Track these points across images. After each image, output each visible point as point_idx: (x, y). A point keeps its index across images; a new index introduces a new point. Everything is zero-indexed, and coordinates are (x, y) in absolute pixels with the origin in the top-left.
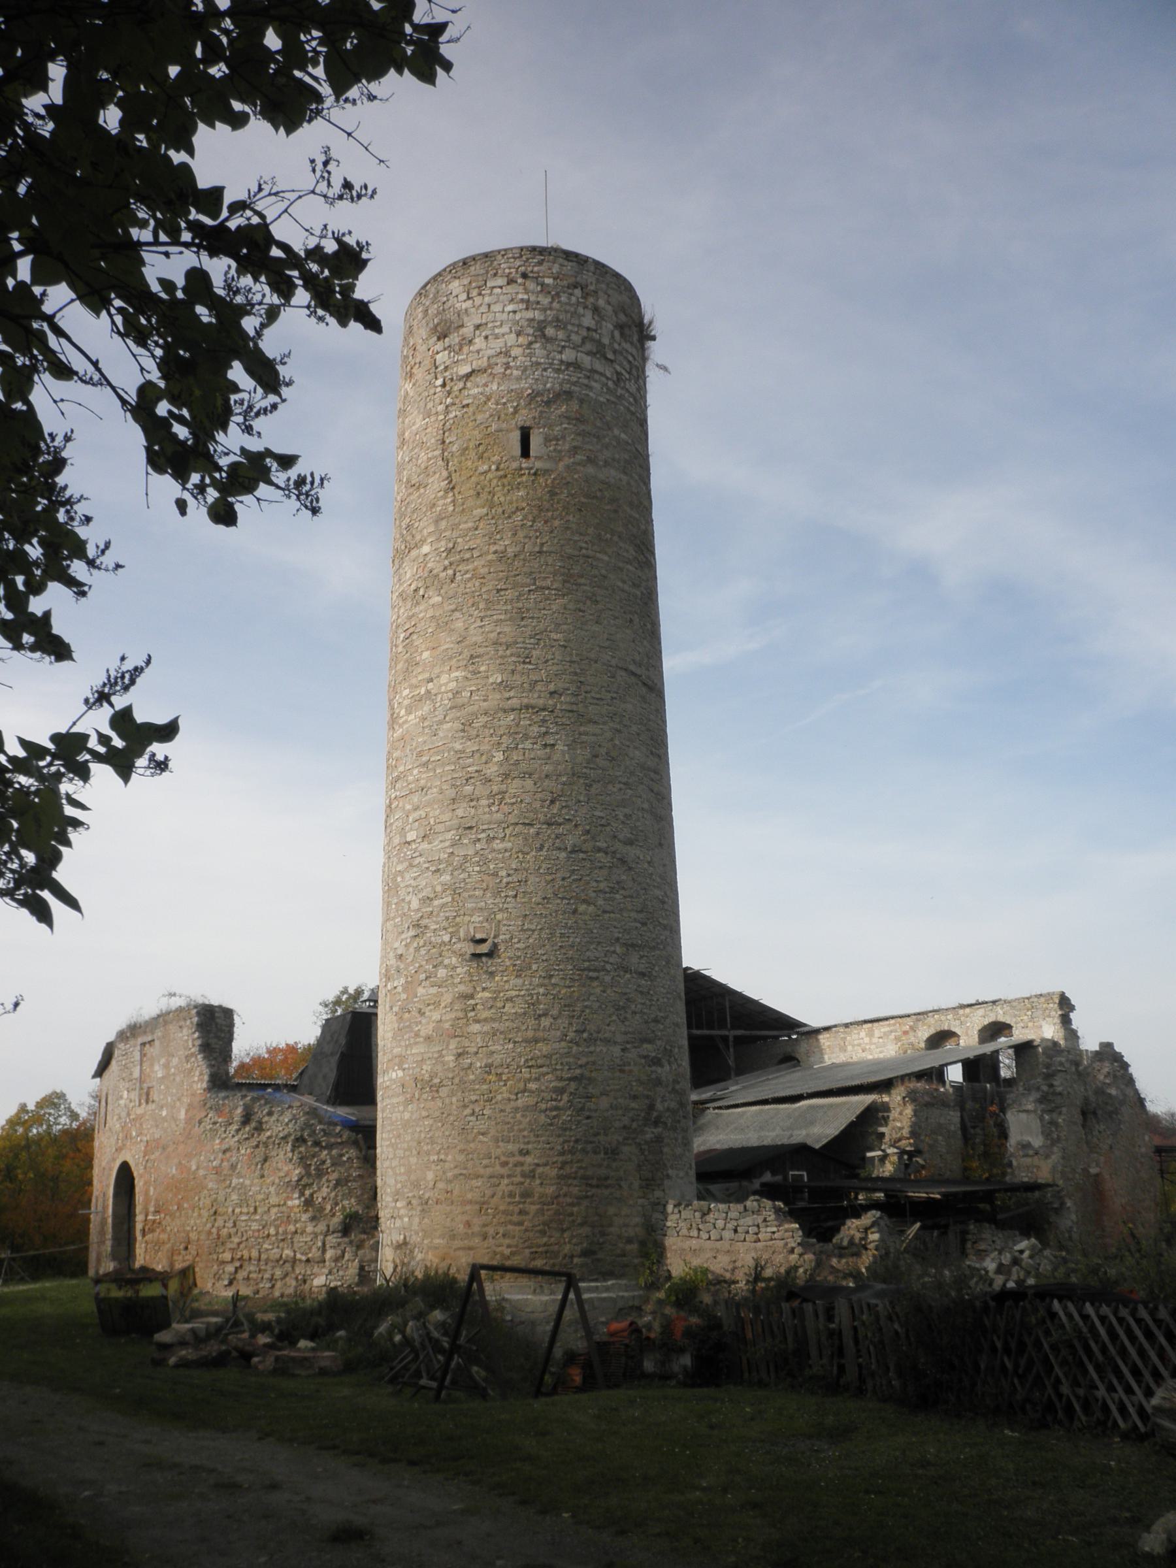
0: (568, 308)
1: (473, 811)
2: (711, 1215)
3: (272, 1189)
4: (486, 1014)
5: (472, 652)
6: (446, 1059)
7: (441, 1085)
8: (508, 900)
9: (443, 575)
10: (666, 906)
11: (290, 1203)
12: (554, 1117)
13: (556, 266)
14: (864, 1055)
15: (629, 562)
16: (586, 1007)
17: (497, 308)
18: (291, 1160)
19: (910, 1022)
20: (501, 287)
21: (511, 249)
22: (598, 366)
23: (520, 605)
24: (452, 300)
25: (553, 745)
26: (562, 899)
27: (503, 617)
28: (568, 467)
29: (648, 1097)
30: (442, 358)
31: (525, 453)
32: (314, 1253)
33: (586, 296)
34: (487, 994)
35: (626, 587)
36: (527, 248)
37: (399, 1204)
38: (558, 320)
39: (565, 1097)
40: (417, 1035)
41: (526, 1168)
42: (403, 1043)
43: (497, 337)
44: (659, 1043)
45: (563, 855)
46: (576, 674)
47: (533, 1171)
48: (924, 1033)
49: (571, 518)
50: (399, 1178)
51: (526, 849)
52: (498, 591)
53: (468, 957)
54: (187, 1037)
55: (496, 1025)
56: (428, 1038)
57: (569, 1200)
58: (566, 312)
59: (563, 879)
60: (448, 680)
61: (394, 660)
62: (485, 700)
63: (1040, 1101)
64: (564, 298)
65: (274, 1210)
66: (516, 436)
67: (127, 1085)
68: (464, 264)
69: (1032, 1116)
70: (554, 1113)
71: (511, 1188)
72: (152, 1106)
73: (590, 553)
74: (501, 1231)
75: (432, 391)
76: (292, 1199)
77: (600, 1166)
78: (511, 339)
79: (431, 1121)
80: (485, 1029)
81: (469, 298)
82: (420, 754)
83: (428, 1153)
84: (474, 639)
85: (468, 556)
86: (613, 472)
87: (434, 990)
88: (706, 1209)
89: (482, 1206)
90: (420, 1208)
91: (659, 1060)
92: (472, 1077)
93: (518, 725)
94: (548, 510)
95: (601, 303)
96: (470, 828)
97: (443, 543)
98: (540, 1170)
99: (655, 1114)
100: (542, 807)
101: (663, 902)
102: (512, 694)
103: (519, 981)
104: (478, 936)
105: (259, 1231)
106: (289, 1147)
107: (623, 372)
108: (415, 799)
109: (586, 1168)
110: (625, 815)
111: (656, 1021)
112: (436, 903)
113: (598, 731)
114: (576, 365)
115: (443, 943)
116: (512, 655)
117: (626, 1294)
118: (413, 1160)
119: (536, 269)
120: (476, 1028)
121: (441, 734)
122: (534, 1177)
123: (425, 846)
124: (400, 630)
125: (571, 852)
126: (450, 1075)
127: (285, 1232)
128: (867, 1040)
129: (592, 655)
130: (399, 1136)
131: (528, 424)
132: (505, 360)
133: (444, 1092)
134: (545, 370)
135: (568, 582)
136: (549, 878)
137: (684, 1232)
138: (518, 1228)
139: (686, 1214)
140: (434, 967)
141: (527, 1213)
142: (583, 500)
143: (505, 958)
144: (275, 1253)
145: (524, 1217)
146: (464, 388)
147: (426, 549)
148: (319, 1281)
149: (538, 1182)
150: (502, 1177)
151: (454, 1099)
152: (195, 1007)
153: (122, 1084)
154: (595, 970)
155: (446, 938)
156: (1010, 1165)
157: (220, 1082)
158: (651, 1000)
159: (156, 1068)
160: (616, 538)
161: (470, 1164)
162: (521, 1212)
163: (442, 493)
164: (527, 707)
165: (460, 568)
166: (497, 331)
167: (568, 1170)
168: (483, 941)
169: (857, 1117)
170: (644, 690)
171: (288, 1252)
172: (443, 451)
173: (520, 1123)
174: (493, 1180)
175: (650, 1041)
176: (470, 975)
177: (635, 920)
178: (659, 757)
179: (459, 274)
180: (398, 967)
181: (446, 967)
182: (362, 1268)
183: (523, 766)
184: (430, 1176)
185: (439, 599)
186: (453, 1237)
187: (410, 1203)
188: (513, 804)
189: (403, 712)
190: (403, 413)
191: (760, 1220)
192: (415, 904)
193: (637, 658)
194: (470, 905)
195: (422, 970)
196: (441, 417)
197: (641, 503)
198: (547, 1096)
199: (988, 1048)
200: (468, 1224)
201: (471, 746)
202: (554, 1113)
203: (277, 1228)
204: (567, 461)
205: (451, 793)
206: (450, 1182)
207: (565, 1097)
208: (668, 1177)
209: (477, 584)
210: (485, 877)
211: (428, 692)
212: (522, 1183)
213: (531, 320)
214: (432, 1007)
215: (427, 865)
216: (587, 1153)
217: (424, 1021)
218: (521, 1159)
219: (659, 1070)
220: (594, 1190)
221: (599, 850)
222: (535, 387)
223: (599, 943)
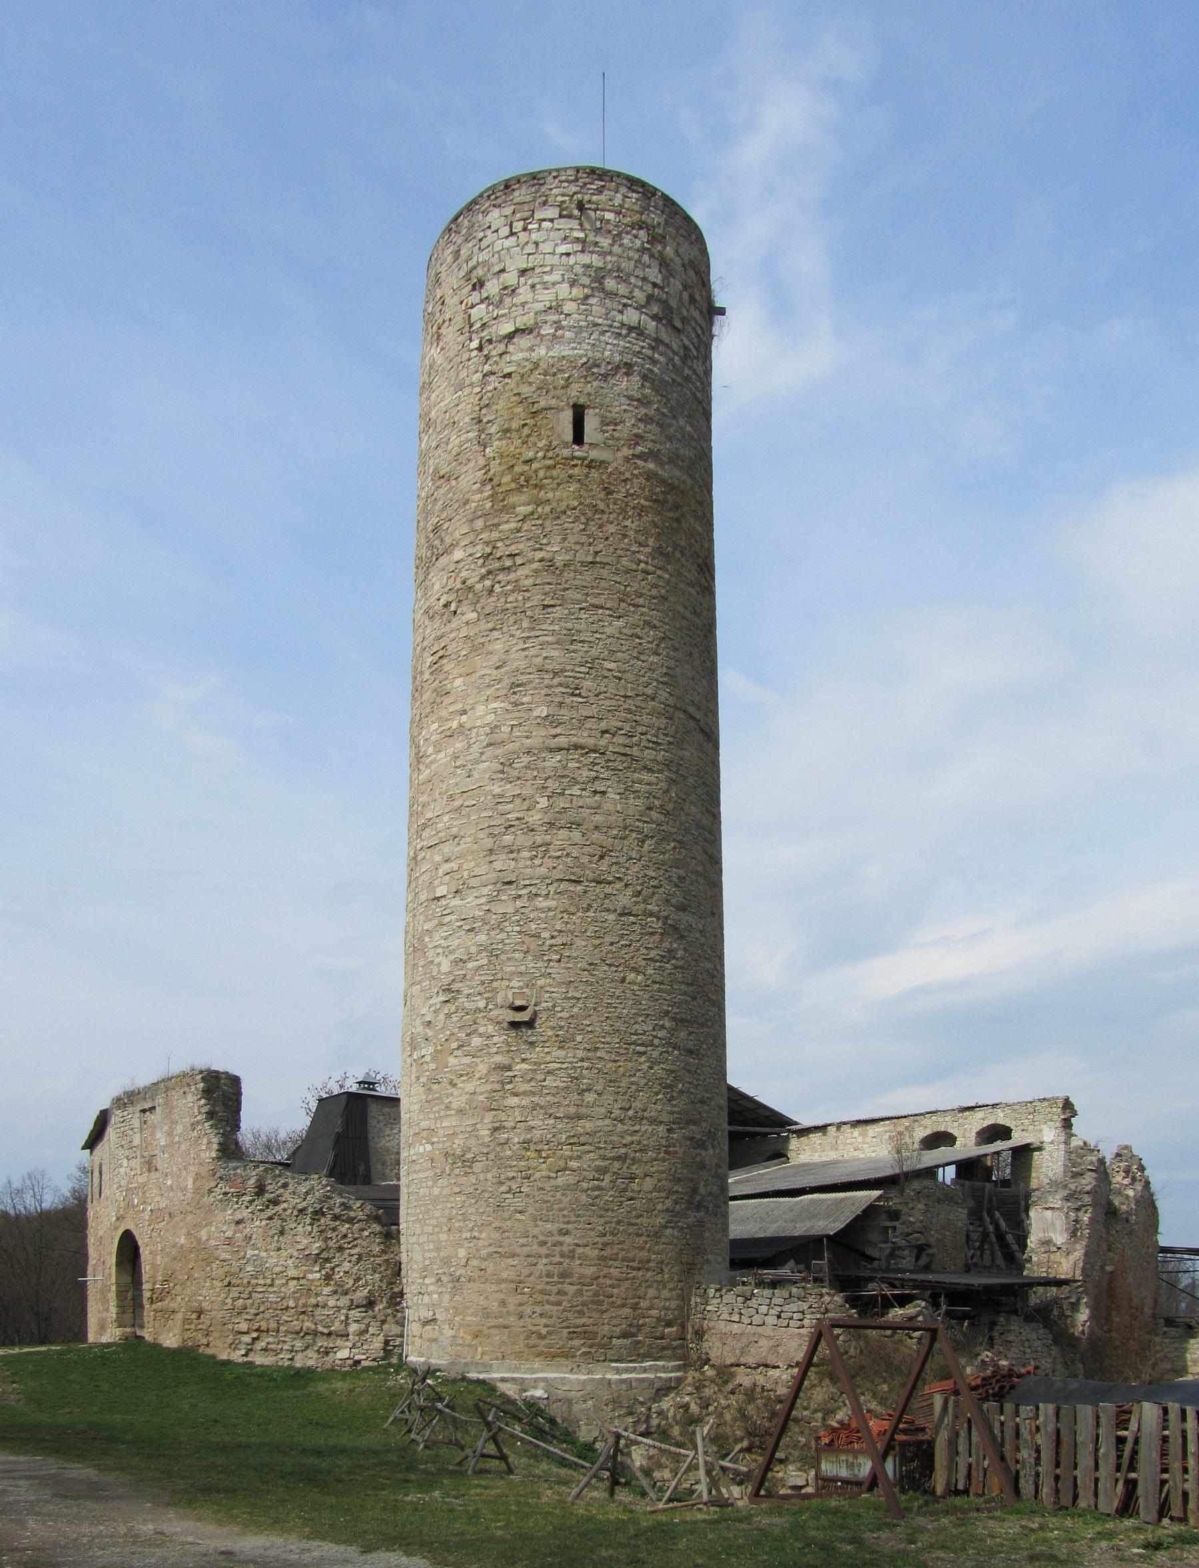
0: (631, 254)
1: (513, 863)
2: (754, 1300)
3: (290, 1262)
4: (526, 1087)
5: (514, 680)
6: (481, 1133)
7: (473, 1160)
8: (552, 964)
9: (479, 587)
10: (715, 981)
11: (310, 1276)
12: (596, 1197)
13: (619, 196)
14: (856, 1153)
15: (690, 584)
16: (632, 1083)
17: (546, 248)
18: (310, 1233)
19: (906, 1122)
20: (552, 220)
21: (565, 169)
22: (665, 336)
23: (569, 626)
24: (491, 237)
25: (603, 793)
26: (610, 965)
27: (549, 639)
28: (627, 460)
29: (691, 1180)
30: (479, 312)
31: (578, 438)
32: (337, 1326)
33: (653, 240)
34: (525, 1066)
35: (688, 614)
36: (584, 168)
37: (427, 1281)
38: (619, 270)
39: (607, 1178)
40: (448, 1108)
41: (565, 1248)
42: (432, 1116)
43: (546, 287)
44: (704, 1124)
45: (612, 917)
46: (629, 711)
47: (573, 1251)
48: (921, 1133)
49: (628, 523)
50: (428, 1255)
51: (572, 909)
52: (546, 607)
53: (505, 1025)
54: (191, 1104)
55: (536, 1099)
56: (460, 1111)
57: (609, 1282)
58: (630, 259)
59: (612, 944)
60: (484, 714)
61: (418, 690)
62: (527, 737)
63: (1067, 1199)
64: (626, 240)
65: (293, 1283)
66: (568, 416)
67: (127, 1153)
68: (507, 187)
69: (1057, 1213)
70: (596, 1193)
71: (550, 1267)
72: (154, 1175)
73: (650, 568)
75: (466, 356)
76: (312, 1272)
77: (642, 1249)
78: (564, 290)
79: (463, 1198)
80: (524, 1103)
81: (512, 234)
82: (451, 798)
83: (460, 1230)
84: (515, 665)
85: (508, 563)
86: (677, 473)
87: (468, 1060)
88: (748, 1294)
89: (517, 1285)
90: (450, 1285)
91: (704, 1142)
92: (509, 1153)
93: (565, 767)
94: (603, 512)
95: (669, 251)
96: (510, 883)
97: (479, 547)
98: (580, 1250)
99: (698, 1198)
100: (590, 862)
101: (713, 977)
102: (558, 730)
103: (562, 1053)
104: (518, 1003)
105: (277, 1303)
106: (308, 1221)
107: (691, 347)
108: (446, 849)
109: (627, 1251)
110: (679, 877)
111: (702, 1102)
112: (470, 965)
113: (653, 780)
114: (637, 330)
115: (478, 1010)
116: (560, 685)
117: (663, 1375)
118: (443, 1237)
119: (594, 198)
120: (513, 1101)
121: (476, 775)
122: (573, 1257)
123: (456, 902)
124: (426, 654)
125: (621, 915)
127: (305, 1305)
128: (860, 1139)
129: (649, 691)
130: (427, 1212)
131: (582, 401)
132: (556, 318)
133: (477, 1167)
134: (603, 333)
135: (623, 601)
136: (597, 942)
137: (725, 1316)
138: (555, 1308)
139: (729, 1297)
140: (468, 1035)
141: (566, 1294)
142: (642, 502)
143: (544, 1028)
144: (296, 1325)
145: (562, 1298)
146: (505, 353)
147: (458, 554)
148: (343, 1354)
151: (489, 1176)
152: (201, 1072)
153: (120, 1152)
154: (642, 1045)
155: (482, 1004)
156: (1029, 1260)
157: (230, 1150)
158: (698, 1080)
159: (159, 1135)
160: (678, 554)
162: (559, 1293)
163: (478, 485)
164: (577, 747)
165: (500, 578)
166: (546, 278)
167: (608, 1252)
168: (522, 1009)
169: (864, 1211)
170: (700, 737)
171: (308, 1325)
172: (481, 431)
173: (561, 1202)
174: (529, 1259)
175: (696, 1123)
176: (508, 1045)
177: (685, 994)
178: (714, 815)
179: (499, 201)
180: (425, 1034)
181: (480, 1035)
182: (387, 1343)
183: (572, 815)
184: (462, 1253)
185: (475, 615)
186: (487, 1315)
187: (439, 1280)
188: (559, 857)
189: (430, 750)
190: (427, 386)
191: (805, 1306)
192: (446, 967)
193: (697, 698)
194: (508, 969)
195: (453, 1038)
196: (477, 390)
197: (705, 515)
200: (503, 1303)
201: (511, 790)
202: (596, 1193)
203: (297, 1300)
204: (626, 452)
205: (489, 843)
206: (485, 1260)
207: (607, 1178)
208: (708, 1261)
209: (520, 598)
210: (526, 939)
211: (461, 726)
212: (561, 1263)
213: (587, 266)
214: (464, 1078)
215: (459, 924)
217: (455, 1093)
218: (561, 1239)
219: (703, 1153)
220: (635, 1273)
221: (651, 915)
222: (590, 354)
223: (648, 1015)
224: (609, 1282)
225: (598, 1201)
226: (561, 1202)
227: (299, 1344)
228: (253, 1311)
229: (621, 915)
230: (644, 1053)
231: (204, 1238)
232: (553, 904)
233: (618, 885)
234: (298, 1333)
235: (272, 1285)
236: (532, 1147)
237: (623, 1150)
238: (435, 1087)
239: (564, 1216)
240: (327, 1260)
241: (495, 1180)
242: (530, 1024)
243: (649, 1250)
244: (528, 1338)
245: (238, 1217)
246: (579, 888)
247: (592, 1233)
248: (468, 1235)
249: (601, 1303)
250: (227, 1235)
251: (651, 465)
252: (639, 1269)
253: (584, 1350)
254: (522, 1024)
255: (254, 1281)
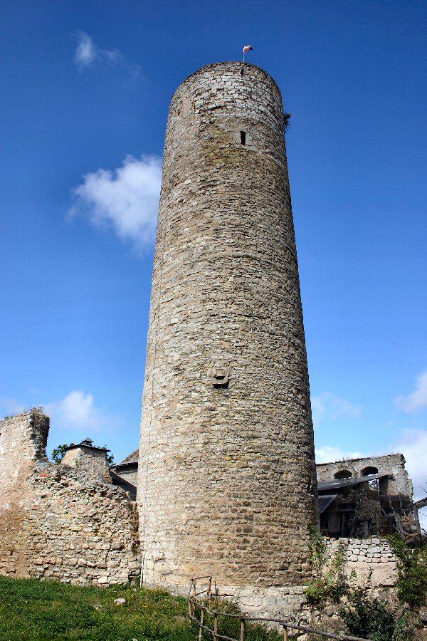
4: (224, 420)
11: (86, 530)
25: (260, 278)
32: (100, 562)
34: (224, 408)
45: (267, 334)
50: (160, 518)
53: (212, 386)
55: (230, 427)
57: (272, 535)
74: (232, 553)
78: (236, 96)
79: (185, 483)
80: (223, 428)
85: (212, 183)
87: (190, 405)
102: (238, 249)
103: (243, 402)
104: (219, 375)
115: (195, 379)
116: (239, 230)
122: (252, 520)
126: (200, 455)
138: (242, 551)
141: (248, 542)
144: (74, 561)
149: (255, 523)
150: (233, 519)
151: (202, 470)
161: (212, 511)
168: (221, 378)
184: (184, 516)
187: (168, 533)
192: (176, 356)
198: (260, 470)
199: (365, 478)
201: (214, 273)
206: (198, 520)
210: (223, 342)
214: (186, 415)
216: (282, 506)
221: (284, 336)
224: (272, 535)
225: (265, 486)
226: (245, 486)
227: (75, 573)
228: (47, 551)
229: (271, 334)
230: (284, 405)
231: (21, 506)
232: (237, 326)
233: (268, 320)
234: (74, 566)
235: (60, 535)
236: (228, 454)
237: (277, 457)
238: (167, 421)
239: (247, 494)
240: (96, 520)
241: (205, 473)
242: (225, 386)
243: (292, 516)
244: (226, 570)
245: (44, 493)
246: (250, 320)
247: (263, 505)
248: (188, 505)
249: (268, 548)
250: (35, 504)
251: (271, 157)
252: (287, 527)
253: (260, 578)
254: (221, 386)
255: (49, 533)
